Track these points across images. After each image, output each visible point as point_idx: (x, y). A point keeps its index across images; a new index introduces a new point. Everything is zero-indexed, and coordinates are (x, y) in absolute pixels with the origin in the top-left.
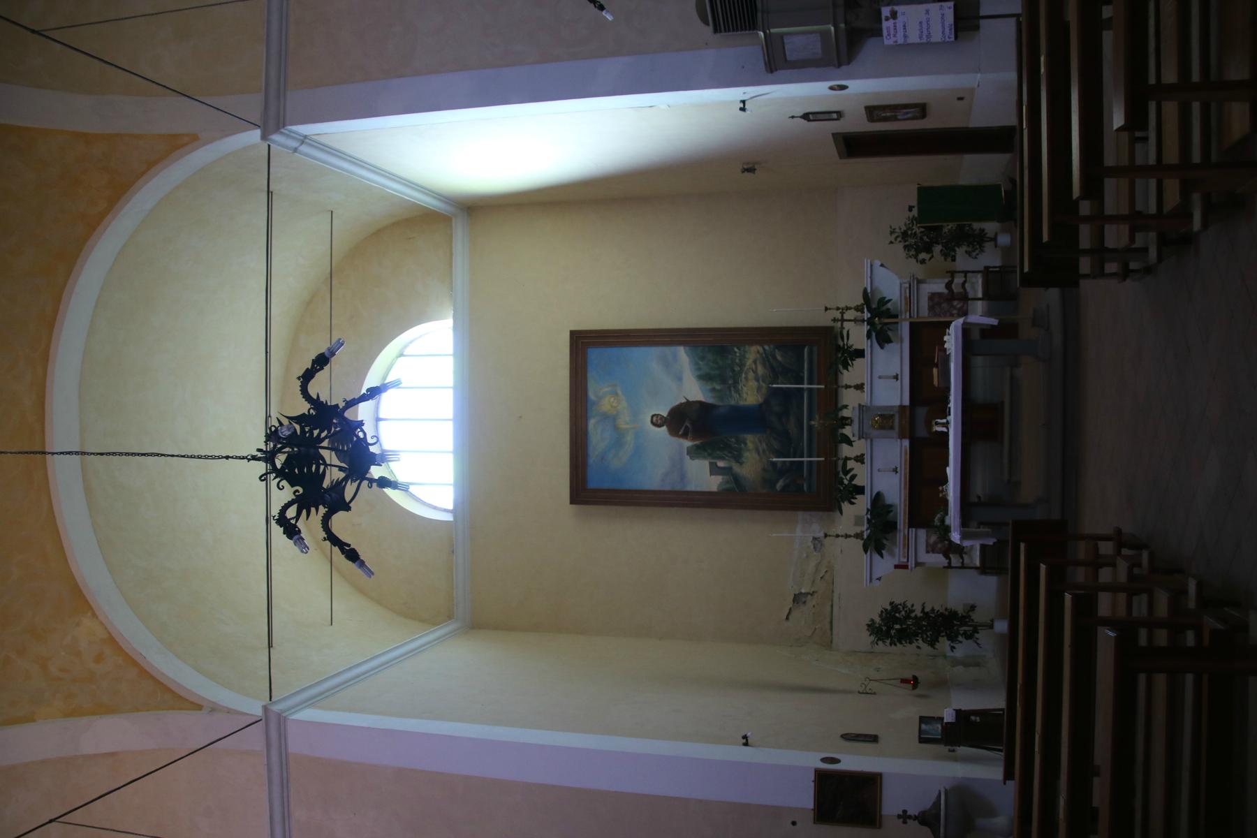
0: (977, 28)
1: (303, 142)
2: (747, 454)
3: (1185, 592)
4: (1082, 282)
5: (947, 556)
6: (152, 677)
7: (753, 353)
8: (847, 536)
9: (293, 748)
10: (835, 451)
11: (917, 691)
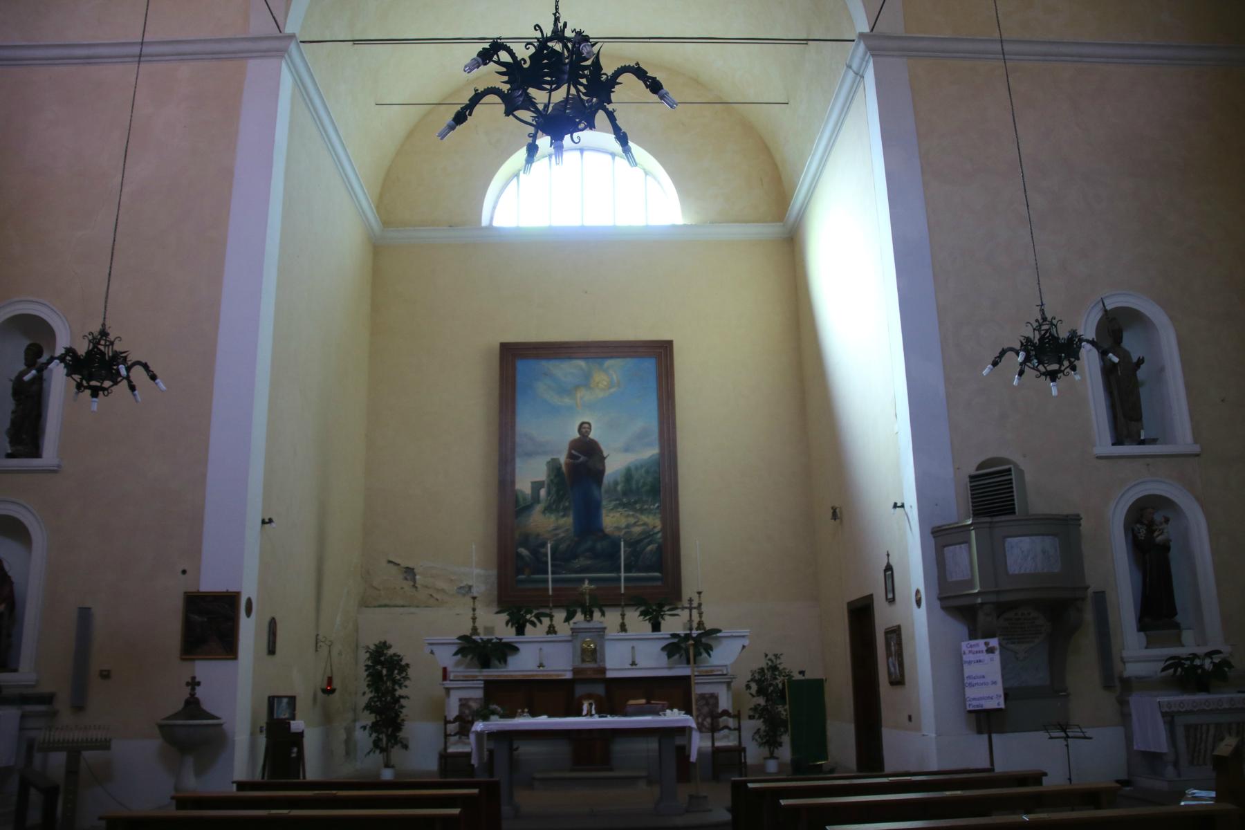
0: (980, 732)
1: (857, 74)
2: (553, 517)
5: (456, 720)
7: (653, 521)
8: (474, 619)
9: (253, 64)
11: (320, 694)
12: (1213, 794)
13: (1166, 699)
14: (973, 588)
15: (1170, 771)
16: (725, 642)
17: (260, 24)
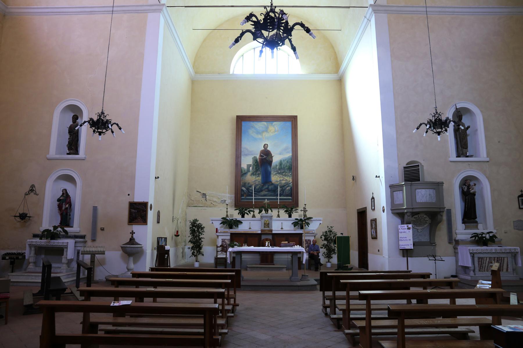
0: (404, 256)
2: (254, 177)
3: (222, 329)
4: (322, 292)
7: (289, 179)
8: (227, 212)
9: (149, 14)
11: (174, 236)
12: (490, 282)
13: (472, 248)
15: (472, 273)
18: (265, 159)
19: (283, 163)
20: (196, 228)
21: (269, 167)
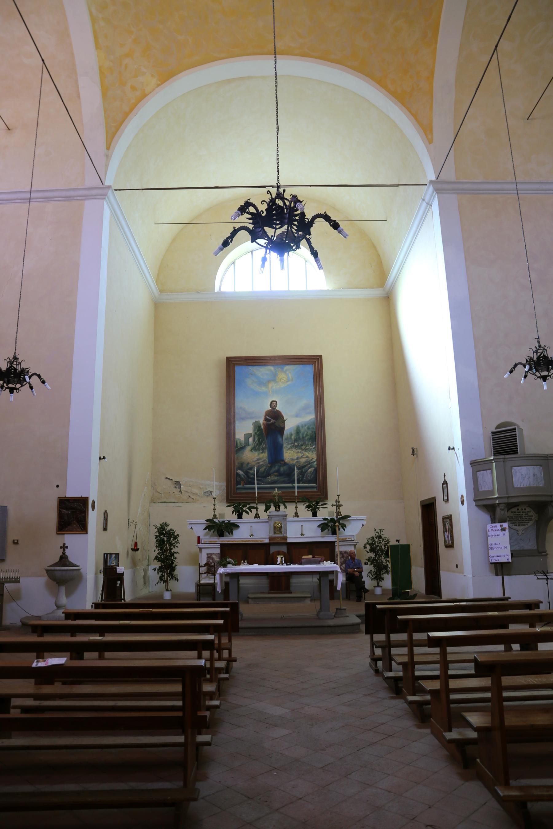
0: (497, 574)
2: (256, 453)
3: (211, 699)
4: (368, 636)
5: (205, 565)
6: (124, 121)
7: (312, 456)
8: (214, 510)
9: (88, 203)
10: (260, 502)
11: (130, 551)
14: (494, 495)
16: (353, 522)
17: (92, 180)
18: (273, 424)
19: (302, 430)
20: (166, 538)
21: (279, 437)
